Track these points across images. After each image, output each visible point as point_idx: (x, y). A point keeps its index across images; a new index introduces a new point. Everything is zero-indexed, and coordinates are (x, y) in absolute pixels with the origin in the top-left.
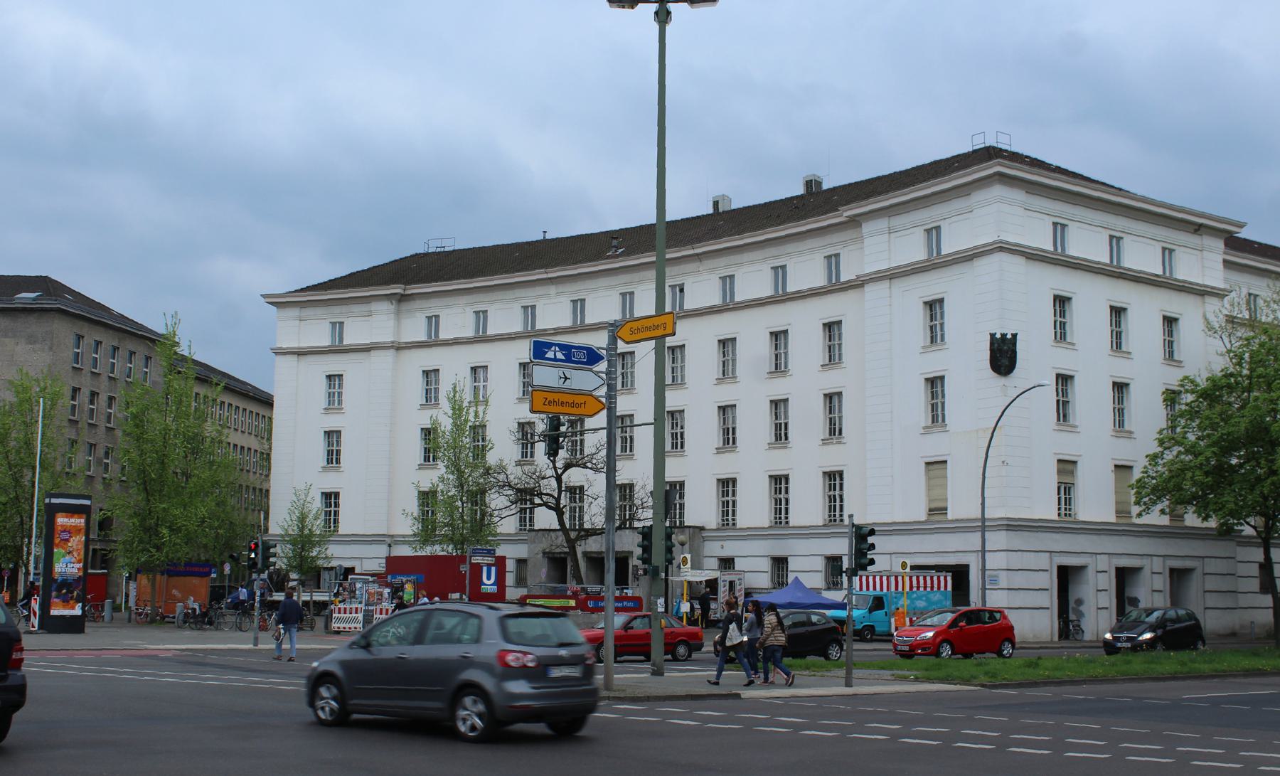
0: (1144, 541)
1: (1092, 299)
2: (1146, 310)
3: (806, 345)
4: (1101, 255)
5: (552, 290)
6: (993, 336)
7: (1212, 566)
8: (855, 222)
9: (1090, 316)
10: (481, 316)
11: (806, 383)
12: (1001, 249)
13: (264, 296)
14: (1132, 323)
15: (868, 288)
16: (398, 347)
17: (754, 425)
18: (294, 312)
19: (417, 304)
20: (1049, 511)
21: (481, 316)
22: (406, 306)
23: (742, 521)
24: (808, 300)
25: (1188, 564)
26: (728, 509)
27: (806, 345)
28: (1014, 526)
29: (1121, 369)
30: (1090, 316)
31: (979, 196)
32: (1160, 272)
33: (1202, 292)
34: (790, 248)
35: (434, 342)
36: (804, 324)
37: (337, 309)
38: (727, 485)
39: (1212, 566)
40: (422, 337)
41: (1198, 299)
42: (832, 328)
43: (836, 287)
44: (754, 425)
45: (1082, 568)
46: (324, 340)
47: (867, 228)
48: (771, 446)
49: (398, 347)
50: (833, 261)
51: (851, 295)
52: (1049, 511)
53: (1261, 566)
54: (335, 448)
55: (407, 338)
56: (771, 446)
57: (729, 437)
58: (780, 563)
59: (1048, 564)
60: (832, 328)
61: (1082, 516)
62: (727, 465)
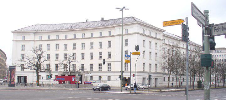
0: (156, 74)
1: (148, 40)
2: (154, 42)
3: (105, 44)
4: (149, 34)
5: (62, 33)
6: (136, 46)
7: (160, 78)
8: (31, 31)
9: (147, 43)
10: (101, 33)
11: (105, 51)
12: (137, 33)
13: (11, 31)
14: (152, 43)
15: (116, 37)
16: (35, 41)
17: (87, 56)
18: (16, 34)
19: (37, 34)
20: (142, 70)
21: (101, 33)
22: (36, 34)
23: (103, 70)
24: (142, 36)
25: (157, 77)
26: (92, 69)
27: (105, 44)
28: (138, 72)
29: (151, 51)
30: (147, 43)
31: (133, 26)
32: (224, 35)
33: (160, 40)
34: (102, 30)
35: (41, 40)
36: (105, 41)
37: (24, 34)
38: (92, 65)
39: (160, 78)
40: (39, 39)
41: (159, 41)
42: (109, 42)
43: (110, 36)
44: (87, 56)
45: (145, 78)
46: (21, 39)
47: (116, 28)
48: (99, 59)
49: (35, 41)
50: (110, 32)
51: (113, 38)
52: (142, 70)
53: (169, 78)
54: (83, 56)
55: (36, 39)
56: (99, 59)
57: (92, 57)
58: (100, 77)
59: (142, 77)
60: (109, 42)
61: (145, 71)
62: (91, 62)
